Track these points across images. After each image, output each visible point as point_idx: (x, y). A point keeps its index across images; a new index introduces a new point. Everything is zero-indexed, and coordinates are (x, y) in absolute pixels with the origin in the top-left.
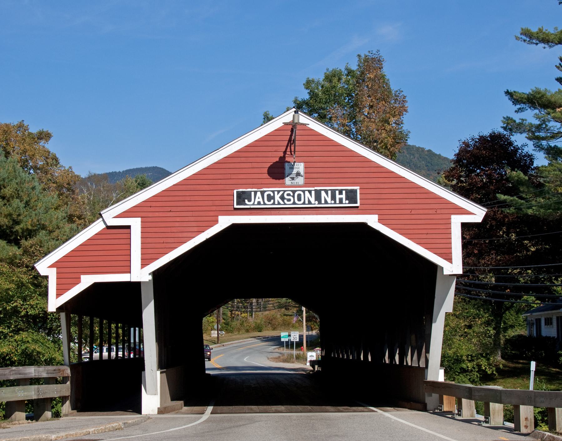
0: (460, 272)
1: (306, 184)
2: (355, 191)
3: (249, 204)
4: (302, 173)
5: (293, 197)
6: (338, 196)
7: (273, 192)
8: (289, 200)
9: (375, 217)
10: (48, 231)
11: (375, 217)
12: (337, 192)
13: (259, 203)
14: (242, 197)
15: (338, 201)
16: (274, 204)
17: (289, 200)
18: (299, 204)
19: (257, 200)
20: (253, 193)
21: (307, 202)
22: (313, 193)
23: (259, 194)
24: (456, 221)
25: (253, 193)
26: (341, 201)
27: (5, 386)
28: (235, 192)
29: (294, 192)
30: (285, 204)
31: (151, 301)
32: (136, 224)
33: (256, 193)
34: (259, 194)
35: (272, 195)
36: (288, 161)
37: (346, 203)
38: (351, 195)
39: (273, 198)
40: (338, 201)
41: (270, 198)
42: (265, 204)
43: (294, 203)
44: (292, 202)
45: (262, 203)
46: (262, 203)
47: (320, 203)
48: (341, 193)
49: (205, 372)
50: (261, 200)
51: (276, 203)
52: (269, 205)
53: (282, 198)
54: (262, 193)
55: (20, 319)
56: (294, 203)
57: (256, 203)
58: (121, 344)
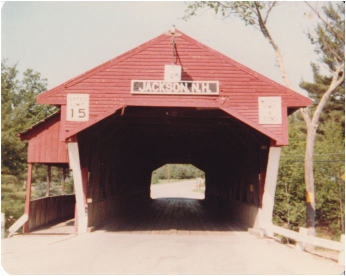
0: (281, 123)
2: (215, 84)
7: (159, 83)
8: (169, 89)
15: (203, 90)
16: (159, 91)
17: (169, 89)
18: (176, 92)
27: (90, 201)
28: (133, 81)
30: (167, 92)
36: (312, 74)
37: (209, 92)
44: (171, 90)
45: (150, 90)
47: (191, 91)
49: (148, 191)
51: (160, 90)
52: (156, 92)
53: (165, 87)
54: (151, 84)
55: (34, 171)
57: (147, 90)
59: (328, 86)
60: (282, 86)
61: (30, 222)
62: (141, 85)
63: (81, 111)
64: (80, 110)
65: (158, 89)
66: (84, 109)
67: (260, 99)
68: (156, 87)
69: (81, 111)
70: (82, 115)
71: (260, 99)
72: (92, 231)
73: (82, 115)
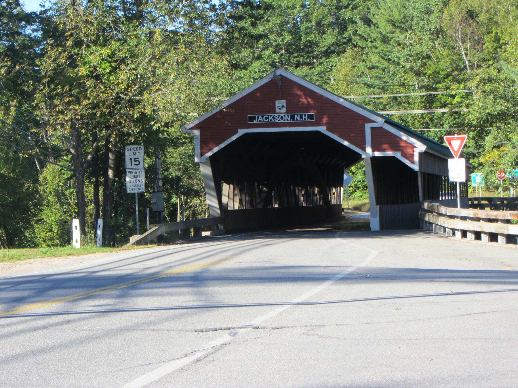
1: (288, 112)
3: (255, 121)
4: (285, 105)
5: (279, 117)
6: (304, 117)
7: (268, 116)
10: (477, 166)
12: (303, 115)
13: (260, 121)
14: (252, 119)
15: (303, 119)
16: (268, 121)
19: (259, 120)
20: (256, 117)
21: (286, 120)
22: (299, 116)
23: (260, 117)
24: (368, 127)
25: (256, 117)
26: (305, 119)
29: (279, 116)
31: (346, 179)
33: (258, 117)
34: (260, 117)
35: (267, 117)
38: (311, 117)
39: (268, 118)
40: (303, 119)
41: (266, 118)
42: (264, 121)
43: (279, 120)
44: (278, 120)
45: (262, 121)
46: (262, 121)
48: (305, 115)
50: (262, 119)
54: (263, 117)
56: (279, 120)
58: (367, 195)
59: (426, 151)
60: (319, 126)
61: (367, 205)
62: (254, 118)
63: (136, 160)
64: (135, 159)
65: (268, 120)
66: (138, 158)
67: (128, 191)
68: (266, 118)
69: (136, 160)
70: (137, 163)
71: (128, 191)
72: (462, 238)
73: (137, 163)
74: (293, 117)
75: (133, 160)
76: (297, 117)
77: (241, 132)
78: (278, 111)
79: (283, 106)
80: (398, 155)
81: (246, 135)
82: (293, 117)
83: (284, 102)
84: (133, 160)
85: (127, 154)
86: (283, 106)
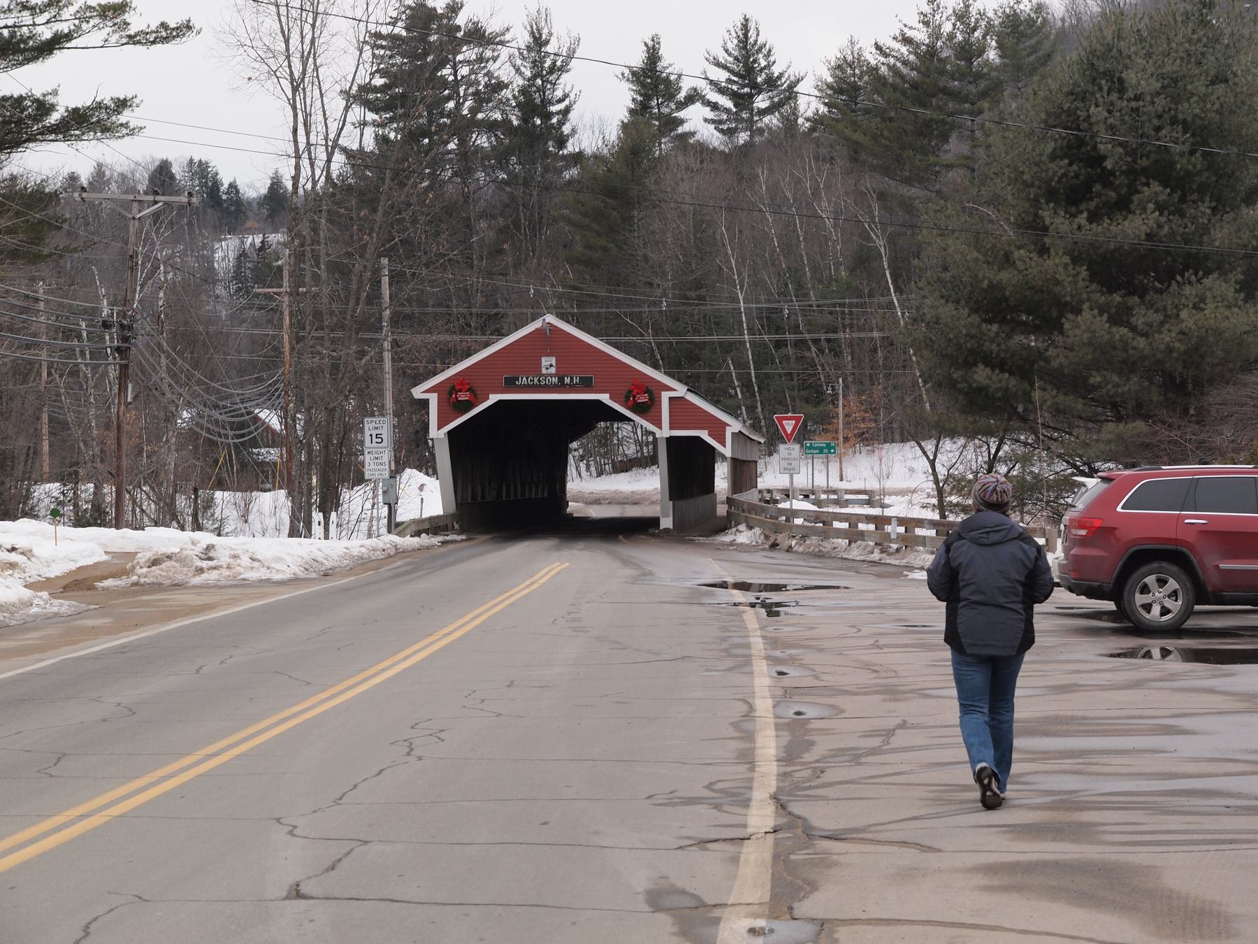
9: (607, 396)
11: (607, 396)
24: (665, 396)
32: (433, 399)
70: (380, 440)
73: (380, 440)
74: (561, 379)
75: (374, 436)
76: (567, 380)
77: (494, 398)
78: (544, 371)
79: (551, 365)
80: (704, 435)
81: (500, 401)
82: (561, 379)
83: (553, 360)
84: (374, 436)
85: (366, 426)
86: (551, 365)
